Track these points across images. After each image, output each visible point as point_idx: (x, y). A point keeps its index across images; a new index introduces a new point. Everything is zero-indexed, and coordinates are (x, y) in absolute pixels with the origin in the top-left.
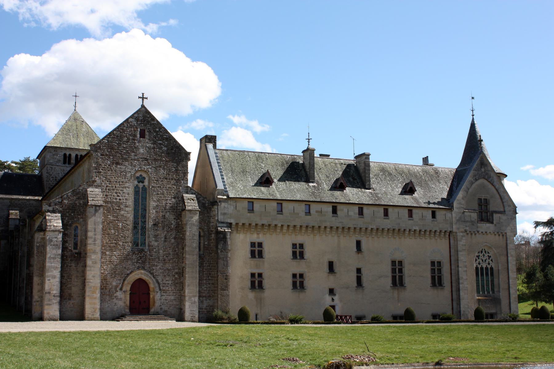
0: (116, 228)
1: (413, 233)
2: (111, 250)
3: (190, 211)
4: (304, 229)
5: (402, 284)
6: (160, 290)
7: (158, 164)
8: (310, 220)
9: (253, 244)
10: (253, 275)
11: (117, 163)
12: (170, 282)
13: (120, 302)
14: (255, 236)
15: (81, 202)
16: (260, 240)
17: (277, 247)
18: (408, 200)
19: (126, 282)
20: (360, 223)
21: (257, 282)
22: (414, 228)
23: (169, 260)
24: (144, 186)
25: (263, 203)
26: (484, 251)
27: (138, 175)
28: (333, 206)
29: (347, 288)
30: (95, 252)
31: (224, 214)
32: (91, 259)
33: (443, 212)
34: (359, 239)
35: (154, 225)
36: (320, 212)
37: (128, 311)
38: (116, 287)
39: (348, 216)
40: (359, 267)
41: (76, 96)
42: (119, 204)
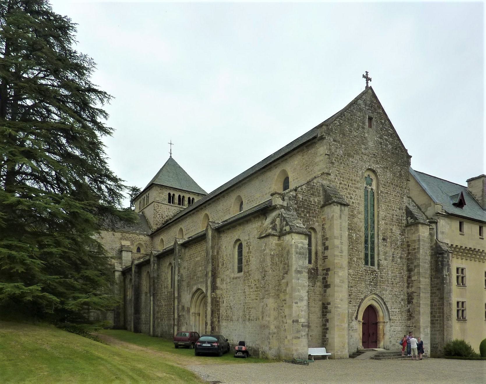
6: (390, 320)
11: (349, 155)
12: (398, 310)
13: (355, 334)
15: (316, 200)
23: (397, 284)
24: (372, 189)
30: (341, 268)
31: (443, 233)
32: (339, 276)
41: (171, 144)
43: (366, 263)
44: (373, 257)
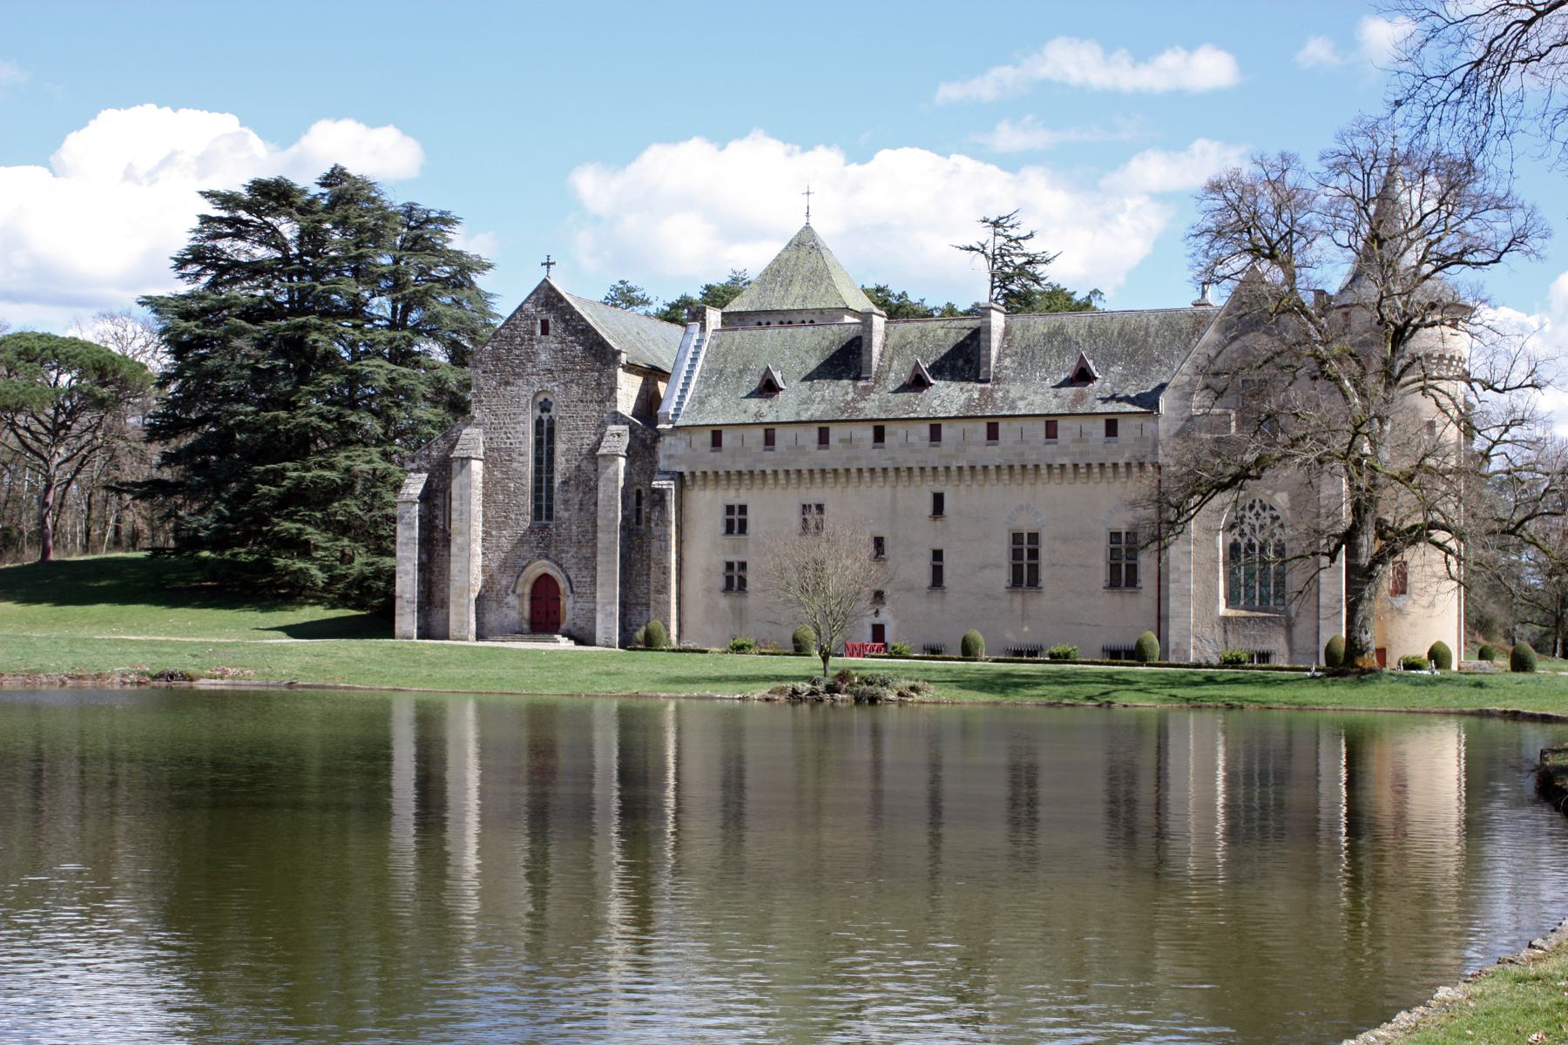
0: (505, 490)
2: (499, 529)
3: (604, 456)
4: (817, 476)
5: (1034, 582)
7: (568, 377)
8: (826, 458)
10: (730, 566)
11: (507, 383)
14: (732, 493)
16: (741, 501)
17: (772, 511)
18: (769, 410)
19: (521, 580)
20: (933, 456)
22: (1059, 461)
25: (739, 432)
26: (1257, 505)
27: (541, 398)
28: (989, 424)
29: (909, 590)
31: (670, 457)
33: (1137, 421)
34: (938, 490)
35: (564, 483)
36: (849, 441)
37: (526, 626)
38: (507, 587)
39: (907, 444)
40: (938, 547)
42: (509, 451)
44: (550, 509)
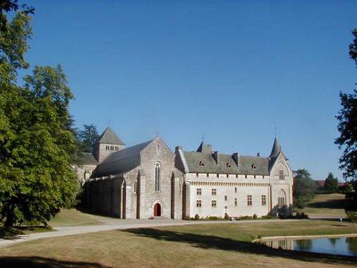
1: (248, 184)
9: (198, 189)
10: (198, 201)
21: (199, 205)
43: (156, 190)
